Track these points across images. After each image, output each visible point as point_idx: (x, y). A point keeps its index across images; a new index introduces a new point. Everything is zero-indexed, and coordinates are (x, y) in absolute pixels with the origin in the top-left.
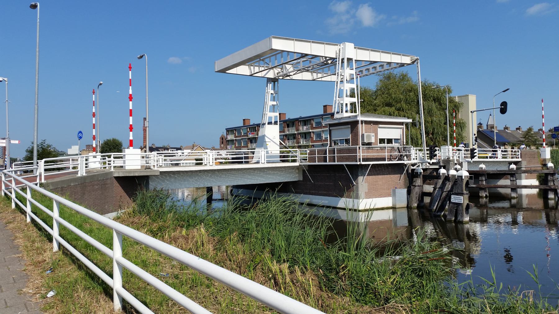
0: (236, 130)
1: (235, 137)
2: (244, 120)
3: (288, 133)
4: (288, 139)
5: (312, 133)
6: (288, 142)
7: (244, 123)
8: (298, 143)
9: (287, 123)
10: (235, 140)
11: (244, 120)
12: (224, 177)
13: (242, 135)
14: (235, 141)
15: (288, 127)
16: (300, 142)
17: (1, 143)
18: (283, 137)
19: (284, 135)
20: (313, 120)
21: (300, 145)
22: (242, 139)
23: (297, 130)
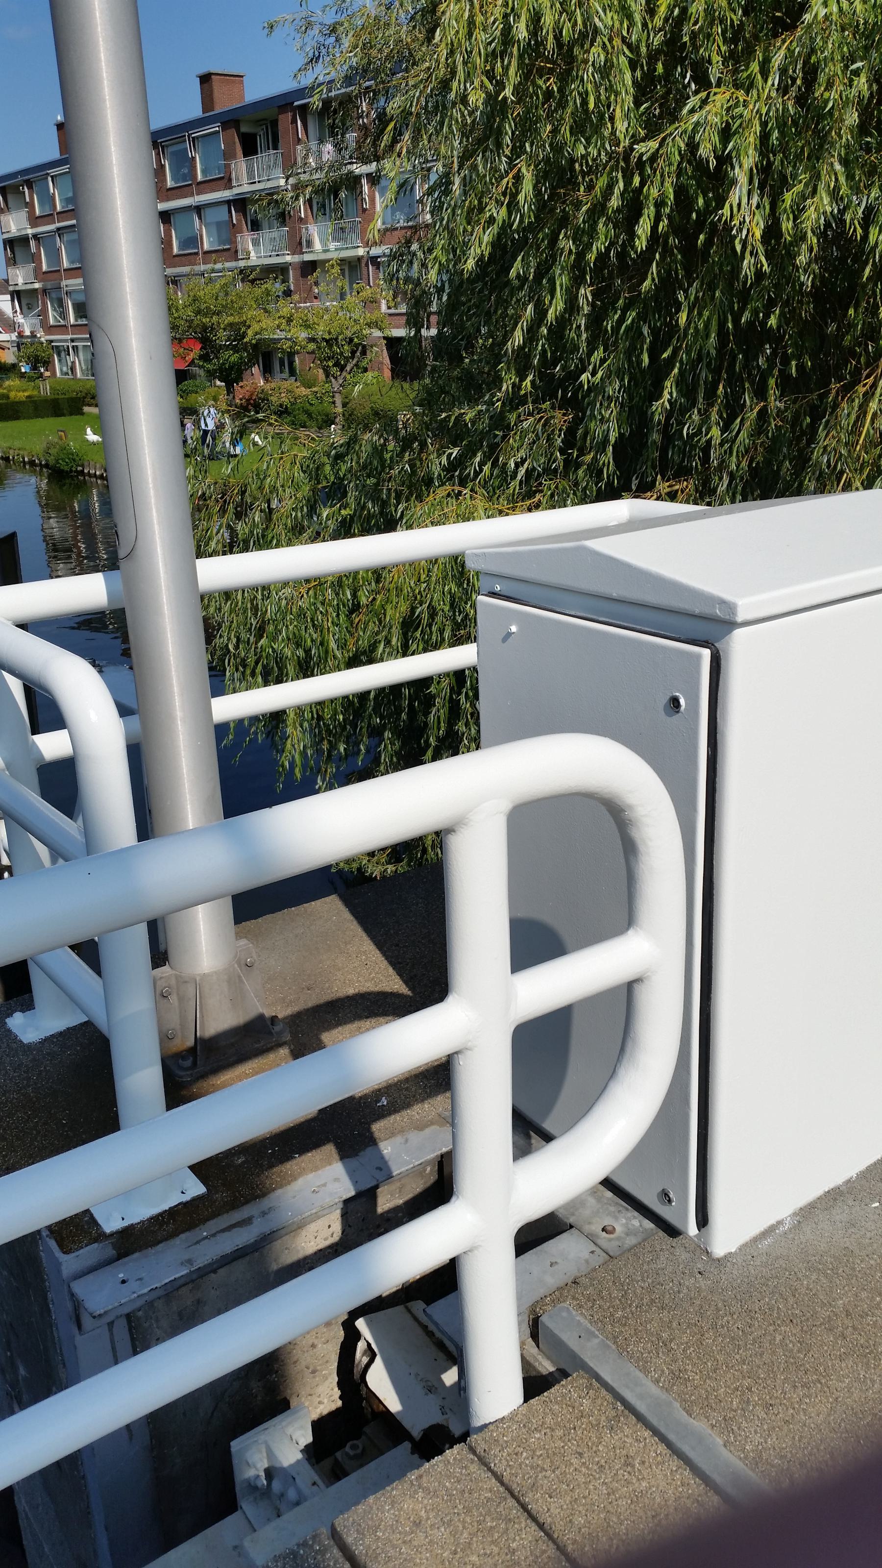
0: (29, 184)
1: (34, 221)
2: (205, 79)
3: (246, 188)
4: (255, 226)
5: (364, 181)
6: (256, 243)
7: (208, 101)
8: (300, 243)
9: (244, 129)
10: (35, 236)
11: (205, 79)
12: (865, 394)
13: (59, 208)
14: (32, 243)
15: (250, 149)
16: (309, 243)
17: (136, 2)
18: (226, 217)
19: (228, 202)
20: (30, 188)
21: (308, 257)
22: (59, 229)
23: (289, 166)
